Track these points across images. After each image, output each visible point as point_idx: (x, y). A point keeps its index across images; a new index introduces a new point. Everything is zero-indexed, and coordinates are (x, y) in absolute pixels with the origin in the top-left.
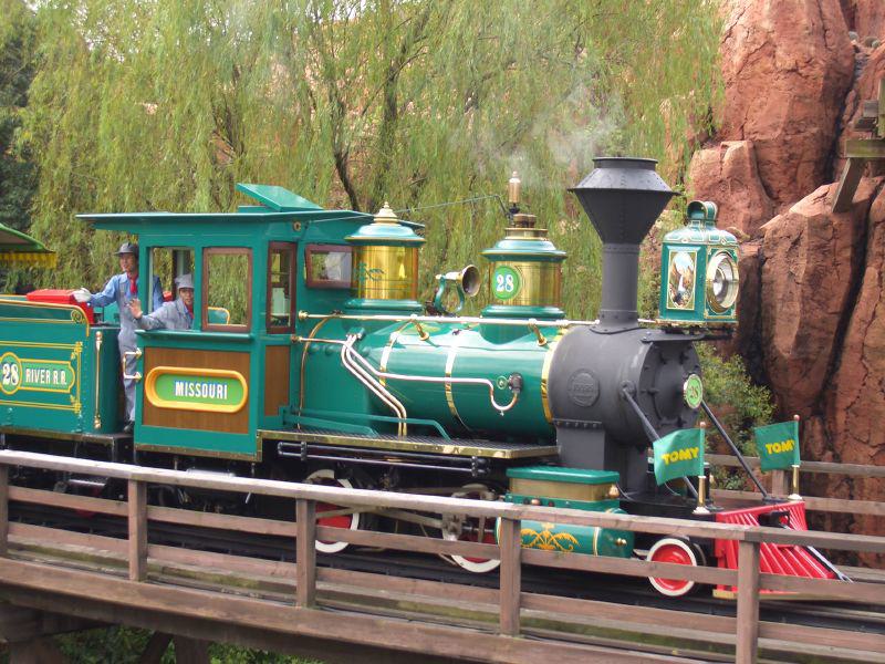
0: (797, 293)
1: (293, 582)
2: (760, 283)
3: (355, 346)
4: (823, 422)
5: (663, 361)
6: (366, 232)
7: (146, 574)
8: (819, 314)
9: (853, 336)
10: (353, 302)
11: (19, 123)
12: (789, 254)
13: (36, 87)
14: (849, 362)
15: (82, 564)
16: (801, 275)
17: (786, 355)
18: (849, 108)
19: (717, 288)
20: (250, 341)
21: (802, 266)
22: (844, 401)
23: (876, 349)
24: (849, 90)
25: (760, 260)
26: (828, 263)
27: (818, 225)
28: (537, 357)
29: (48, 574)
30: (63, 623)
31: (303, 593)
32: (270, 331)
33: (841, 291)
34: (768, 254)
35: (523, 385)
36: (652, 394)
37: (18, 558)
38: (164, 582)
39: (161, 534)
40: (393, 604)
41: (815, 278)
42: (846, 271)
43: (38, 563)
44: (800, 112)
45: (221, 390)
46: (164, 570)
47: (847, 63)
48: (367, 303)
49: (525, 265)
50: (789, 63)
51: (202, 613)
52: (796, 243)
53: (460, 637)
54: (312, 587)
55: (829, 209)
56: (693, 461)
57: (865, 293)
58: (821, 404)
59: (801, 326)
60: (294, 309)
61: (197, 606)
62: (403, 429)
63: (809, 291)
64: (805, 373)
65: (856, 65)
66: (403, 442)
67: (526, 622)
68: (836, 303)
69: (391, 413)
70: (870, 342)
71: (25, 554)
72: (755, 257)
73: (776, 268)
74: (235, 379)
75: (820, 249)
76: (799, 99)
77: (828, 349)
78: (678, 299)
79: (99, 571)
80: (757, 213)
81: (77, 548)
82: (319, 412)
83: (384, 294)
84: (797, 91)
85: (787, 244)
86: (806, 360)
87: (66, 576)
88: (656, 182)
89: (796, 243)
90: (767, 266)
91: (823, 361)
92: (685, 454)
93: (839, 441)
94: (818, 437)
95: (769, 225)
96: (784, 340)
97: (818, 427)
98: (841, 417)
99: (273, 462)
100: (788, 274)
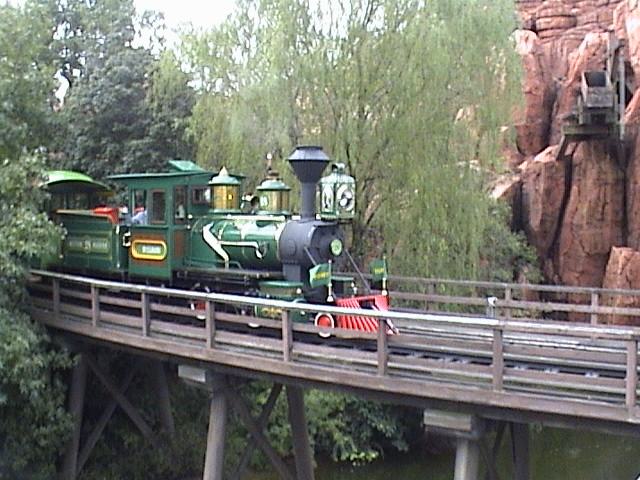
0: (540, 200)
1: (376, 363)
2: (521, 195)
3: (210, 229)
4: (553, 261)
5: (323, 234)
6: (215, 180)
7: (215, 344)
8: (550, 209)
9: (567, 219)
10: (211, 211)
11: (188, 125)
12: (534, 180)
13: (195, 109)
14: (565, 233)
15: (256, 352)
16: (541, 191)
17: (536, 230)
18: (555, 110)
19: (343, 202)
20: (167, 229)
21: (542, 186)
22: (563, 250)
23: (577, 226)
24: (554, 101)
25: (521, 183)
26: (554, 185)
27: (548, 166)
28: (273, 232)
29: (239, 358)
30: (238, 379)
31: (381, 368)
32: (175, 224)
33: (560, 197)
34: (525, 181)
35: (270, 244)
36: (318, 249)
37: (221, 349)
38: (301, 362)
39: (220, 325)
40: (429, 373)
41: (548, 192)
42: (562, 188)
43: (232, 351)
44: (534, 112)
45: (157, 250)
46: (300, 355)
47: (553, 89)
48: (216, 211)
49: (274, 193)
50: (527, 89)
51: (326, 379)
52: (538, 175)
53: (472, 391)
54: (386, 365)
55: (554, 159)
56: (326, 278)
57: (572, 198)
58: (552, 252)
59: (543, 214)
60: (187, 215)
61: (324, 375)
62: (227, 265)
63: (545, 198)
64: (544, 238)
65: (557, 90)
66: (227, 270)
67: (505, 382)
68: (558, 204)
69: (223, 259)
70: (575, 222)
71: (223, 346)
72: (519, 182)
73: (528, 187)
74: (161, 245)
75: (550, 178)
76: (532, 106)
77: (555, 226)
78: (326, 207)
79: (266, 357)
80: (515, 161)
81: (250, 344)
82: (203, 259)
83: (225, 207)
84: (532, 102)
85: (534, 176)
86: (545, 232)
87: (249, 359)
88: (321, 156)
89: (538, 175)
90: (524, 186)
91: (553, 231)
92: (323, 275)
93: (561, 271)
94: (551, 269)
95: (523, 167)
96: (534, 222)
97: (551, 264)
98: (562, 258)
99: (176, 282)
100: (535, 191)
